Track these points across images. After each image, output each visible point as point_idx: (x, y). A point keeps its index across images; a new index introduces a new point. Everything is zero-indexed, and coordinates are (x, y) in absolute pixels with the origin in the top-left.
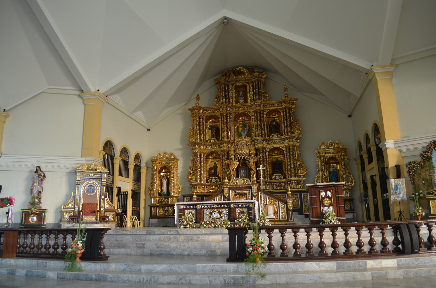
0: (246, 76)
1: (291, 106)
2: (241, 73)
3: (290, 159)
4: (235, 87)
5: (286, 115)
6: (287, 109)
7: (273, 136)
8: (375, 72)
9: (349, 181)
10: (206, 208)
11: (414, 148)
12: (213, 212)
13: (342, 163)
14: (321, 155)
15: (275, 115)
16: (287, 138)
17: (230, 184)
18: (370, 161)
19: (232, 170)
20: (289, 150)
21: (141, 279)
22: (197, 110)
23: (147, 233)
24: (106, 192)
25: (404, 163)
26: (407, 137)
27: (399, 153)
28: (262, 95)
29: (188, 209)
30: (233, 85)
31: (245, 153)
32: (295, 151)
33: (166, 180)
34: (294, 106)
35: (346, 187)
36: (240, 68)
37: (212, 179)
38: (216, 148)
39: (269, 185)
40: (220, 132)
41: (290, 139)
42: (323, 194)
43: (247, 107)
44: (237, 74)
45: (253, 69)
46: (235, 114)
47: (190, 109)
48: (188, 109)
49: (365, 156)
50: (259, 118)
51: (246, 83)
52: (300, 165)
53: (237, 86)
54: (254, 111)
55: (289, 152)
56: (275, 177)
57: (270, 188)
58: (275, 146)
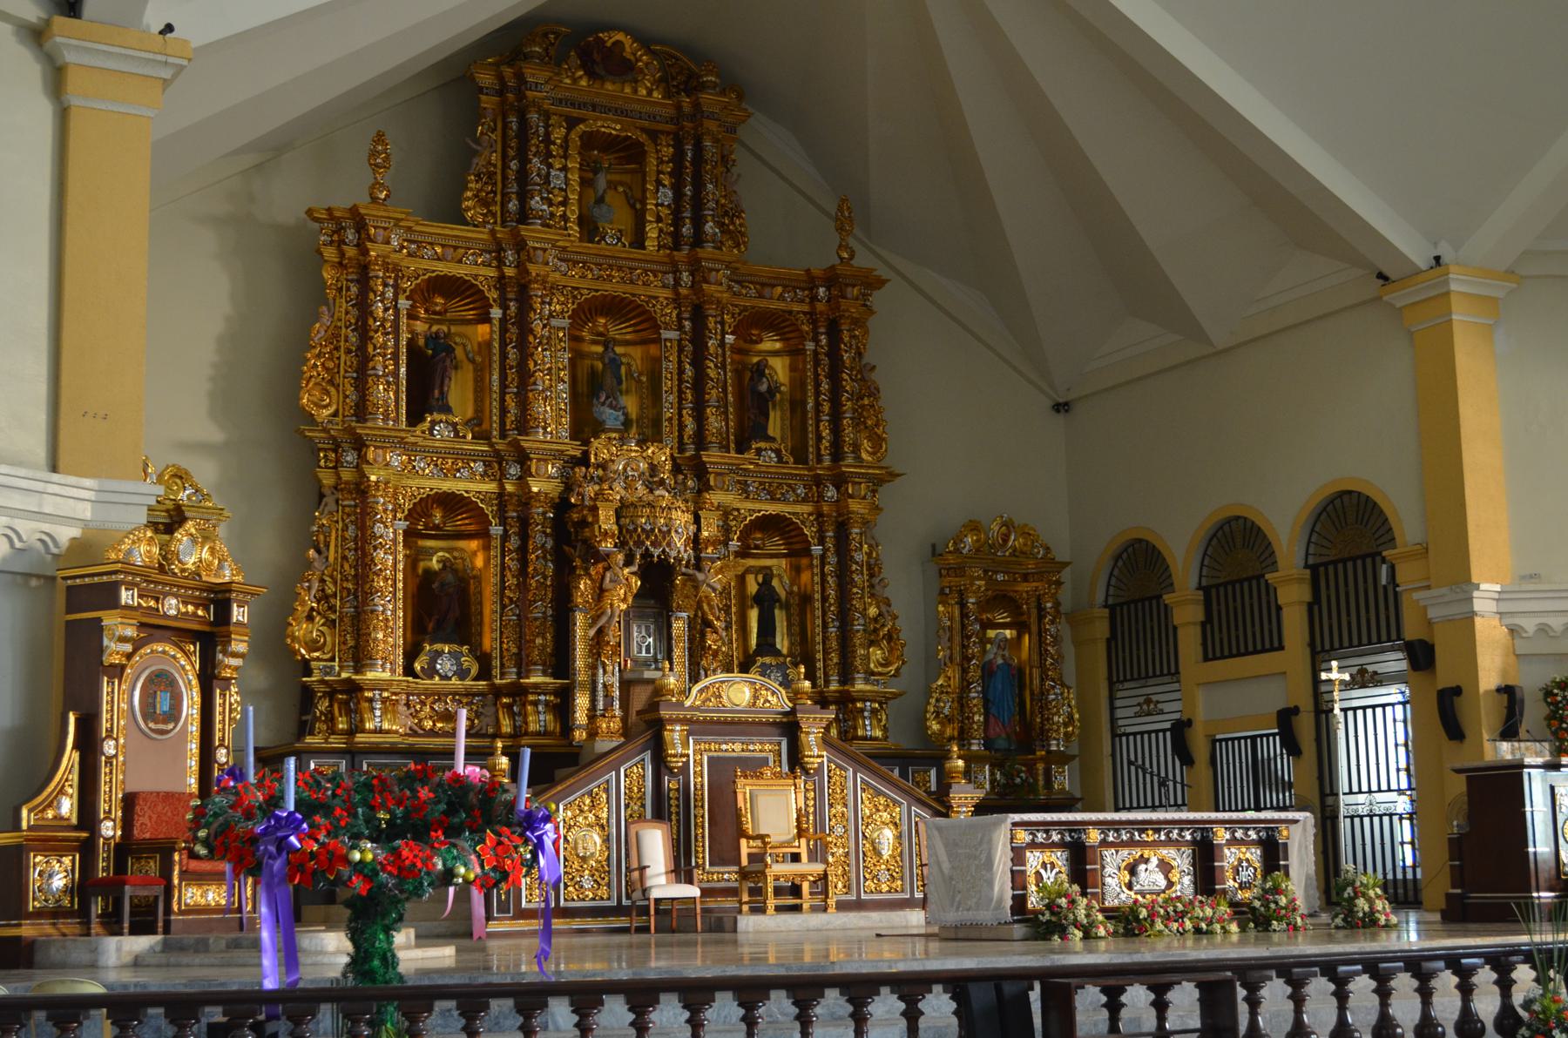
0: (568, 81)
2: (623, 69)
4: (581, 137)
10: (1112, 845)
11: (1564, 625)
22: (381, 231)
25: (1532, 681)
26: (1533, 577)
27: (1509, 638)
29: (1041, 846)
31: (652, 530)
35: (1058, 745)
36: (620, 36)
41: (857, 487)
43: (646, 271)
46: (575, 297)
48: (888, 281)
51: (643, 130)
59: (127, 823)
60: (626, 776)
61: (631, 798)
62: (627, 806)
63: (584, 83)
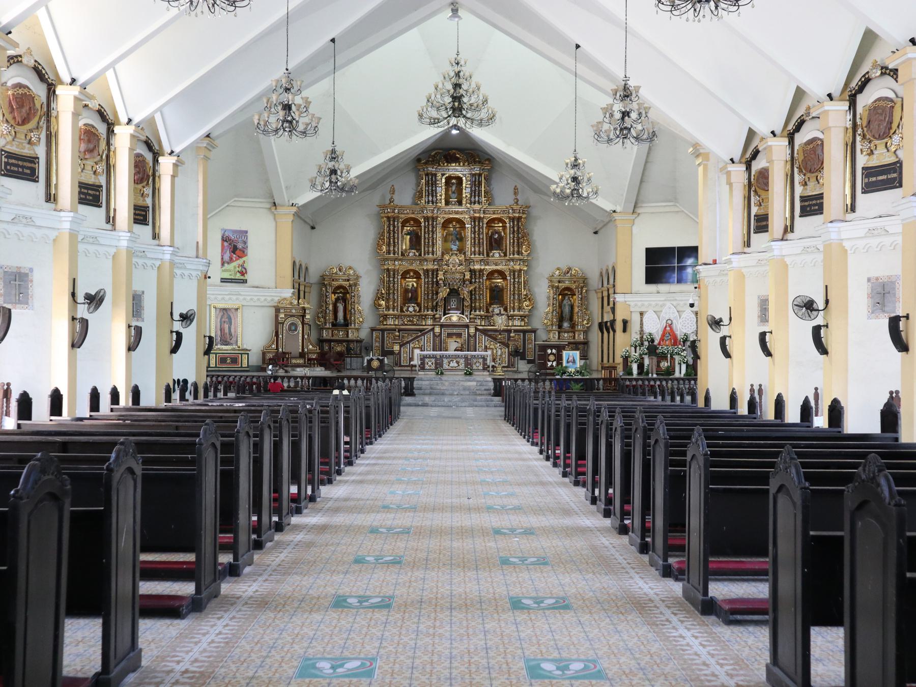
3: (514, 287)
5: (513, 227)
16: (513, 260)
20: (514, 275)
30: (443, 175)
34: (524, 216)
36: (454, 151)
38: (415, 266)
42: (549, 351)
47: (379, 206)
54: (471, 218)
55: (514, 279)
58: (494, 267)
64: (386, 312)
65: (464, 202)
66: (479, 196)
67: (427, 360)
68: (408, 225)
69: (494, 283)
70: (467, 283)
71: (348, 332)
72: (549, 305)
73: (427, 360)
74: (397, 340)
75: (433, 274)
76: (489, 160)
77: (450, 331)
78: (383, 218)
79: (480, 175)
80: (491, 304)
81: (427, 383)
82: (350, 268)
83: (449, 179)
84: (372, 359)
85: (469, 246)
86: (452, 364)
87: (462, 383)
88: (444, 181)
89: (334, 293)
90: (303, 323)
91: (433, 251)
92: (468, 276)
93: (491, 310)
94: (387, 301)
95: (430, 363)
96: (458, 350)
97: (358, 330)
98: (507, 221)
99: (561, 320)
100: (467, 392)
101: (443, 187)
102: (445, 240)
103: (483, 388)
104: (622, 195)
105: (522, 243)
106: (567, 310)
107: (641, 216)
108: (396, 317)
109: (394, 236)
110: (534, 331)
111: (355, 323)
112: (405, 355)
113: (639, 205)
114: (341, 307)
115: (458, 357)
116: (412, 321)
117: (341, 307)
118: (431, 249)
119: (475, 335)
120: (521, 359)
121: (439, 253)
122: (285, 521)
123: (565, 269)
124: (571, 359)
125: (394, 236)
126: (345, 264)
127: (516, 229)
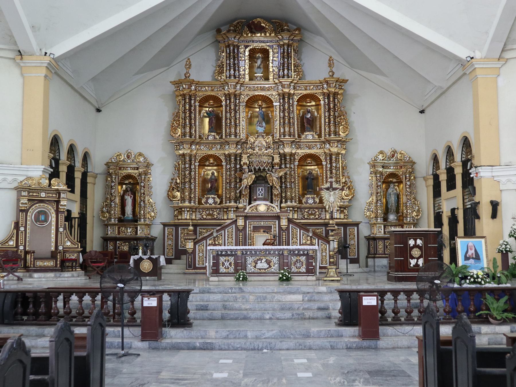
1: (337, 90)
5: (329, 104)
6: (331, 96)
7: (306, 135)
8: (476, 66)
9: (414, 211)
12: (258, 260)
13: (406, 184)
14: (377, 170)
15: (311, 102)
17: (246, 211)
18: (451, 186)
19: (244, 188)
20: (331, 159)
21: (256, 345)
22: (187, 86)
23: (200, 291)
24: (65, 221)
28: (293, 68)
30: (246, 47)
31: (261, 162)
32: (339, 161)
33: (131, 197)
36: (259, 19)
37: (208, 198)
38: (215, 151)
39: (298, 212)
40: (224, 124)
41: (334, 144)
42: (412, 242)
44: (254, 30)
45: (279, 23)
47: (174, 83)
48: (171, 82)
49: (443, 177)
50: (286, 105)
51: (268, 46)
52: (344, 183)
53: (252, 49)
54: (279, 95)
55: (331, 163)
56: (307, 201)
57: (299, 216)
58: (308, 151)
59: (25, 246)
60: (227, 232)
61: (229, 237)
62: (228, 240)
63: (250, 35)
64: (180, 205)
65: (271, 77)
66: (288, 70)
67: (222, 259)
68: (206, 105)
69: (307, 170)
70: (276, 167)
71: (137, 228)
72: (371, 195)
73: (222, 259)
74: (191, 235)
75: (236, 159)
76: (299, 29)
77: (257, 223)
78: (177, 96)
79: (289, 45)
80: (303, 195)
81: (218, 297)
82: (140, 154)
83: (253, 52)
84: (141, 259)
85: (278, 127)
86: (260, 265)
87: (278, 297)
88: (247, 53)
89: (121, 184)
90: (57, 212)
91: (236, 133)
92: (277, 160)
93: (304, 200)
94: (183, 192)
95: (227, 264)
96: (268, 244)
97: (149, 226)
98: (321, 98)
99: (387, 212)
100: (288, 314)
101: (247, 61)
102: (250, 122)
103: (315, 306)
104: (487, 33)
105: (340, 123)
106: (392, 199)
107: (510, 63)
108: (192, 210)
109: (190, 116)
110: (357, 225)
111: (145, 218)
112: (201, 255)
113: (509, 47)
114: (129, 200)
115: (267, 253)
116: (212, 215)
117: (129, 200)
118: (233, 130)
119: (288, 228)
120: (342, 258)
121: (243, 136)
122: (240, 282)
123: (389, 153)
124: (471, 252)
125: (190, 116)
126: (135, 151)
127: (332, 106)
